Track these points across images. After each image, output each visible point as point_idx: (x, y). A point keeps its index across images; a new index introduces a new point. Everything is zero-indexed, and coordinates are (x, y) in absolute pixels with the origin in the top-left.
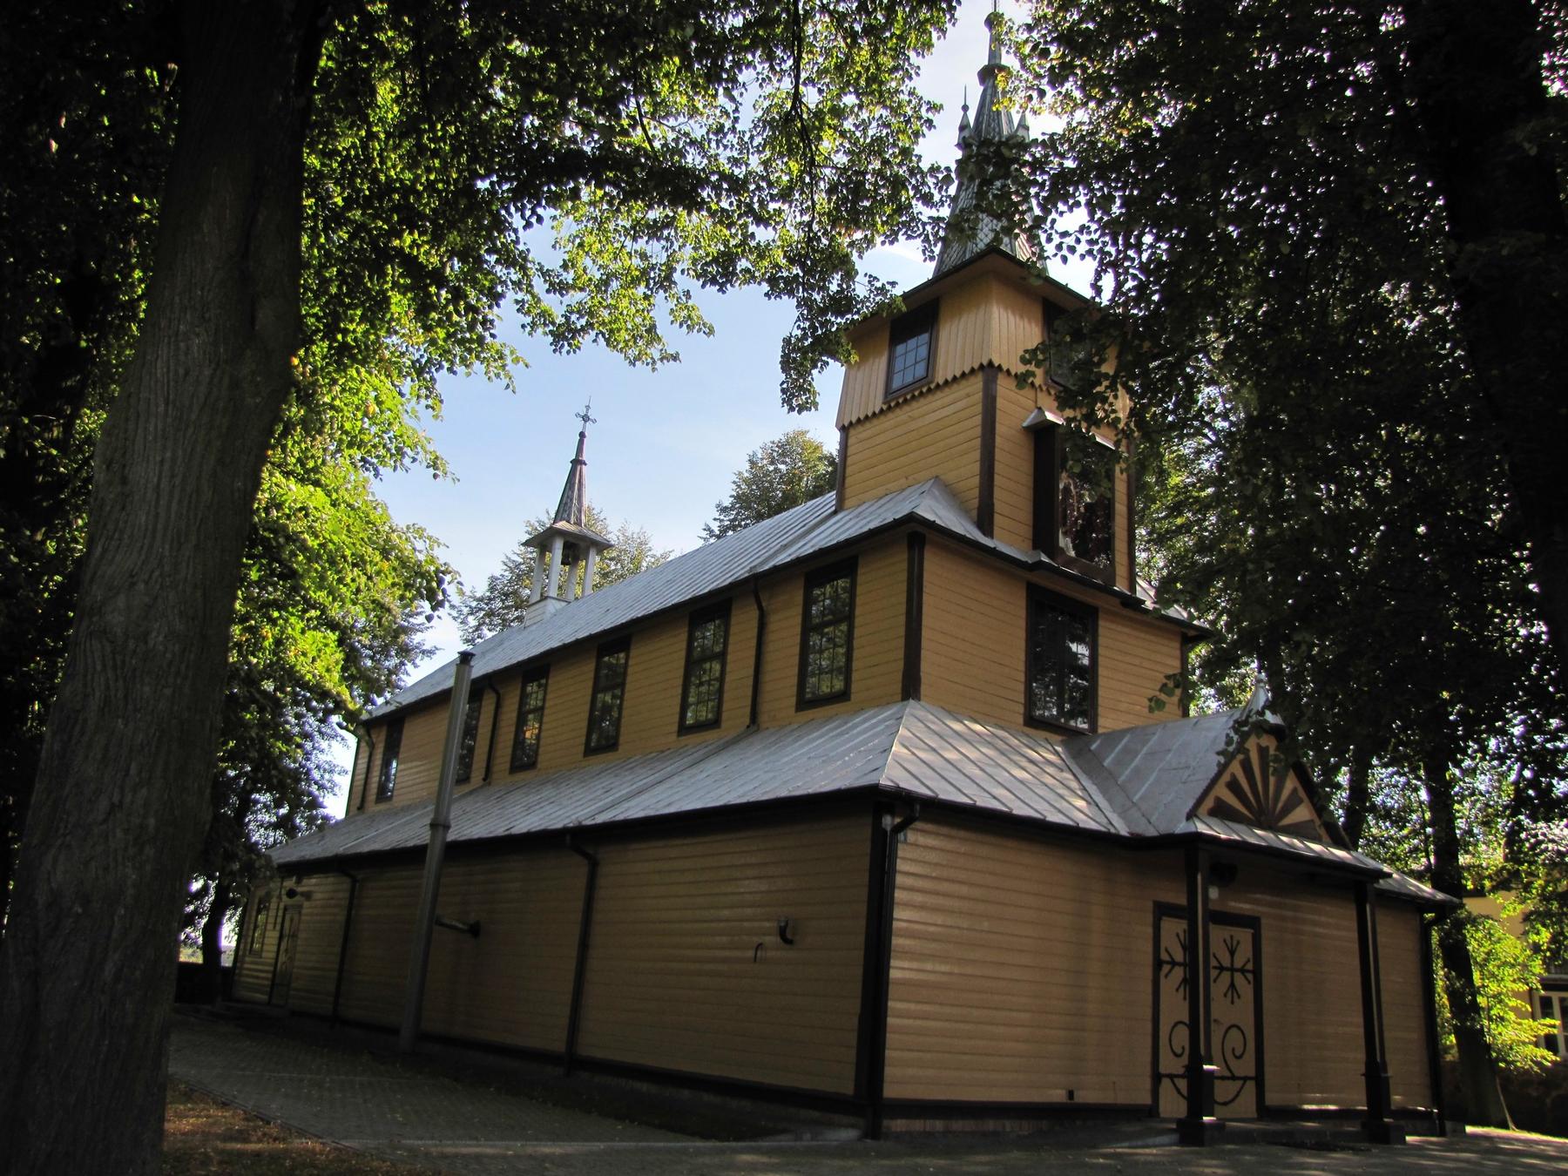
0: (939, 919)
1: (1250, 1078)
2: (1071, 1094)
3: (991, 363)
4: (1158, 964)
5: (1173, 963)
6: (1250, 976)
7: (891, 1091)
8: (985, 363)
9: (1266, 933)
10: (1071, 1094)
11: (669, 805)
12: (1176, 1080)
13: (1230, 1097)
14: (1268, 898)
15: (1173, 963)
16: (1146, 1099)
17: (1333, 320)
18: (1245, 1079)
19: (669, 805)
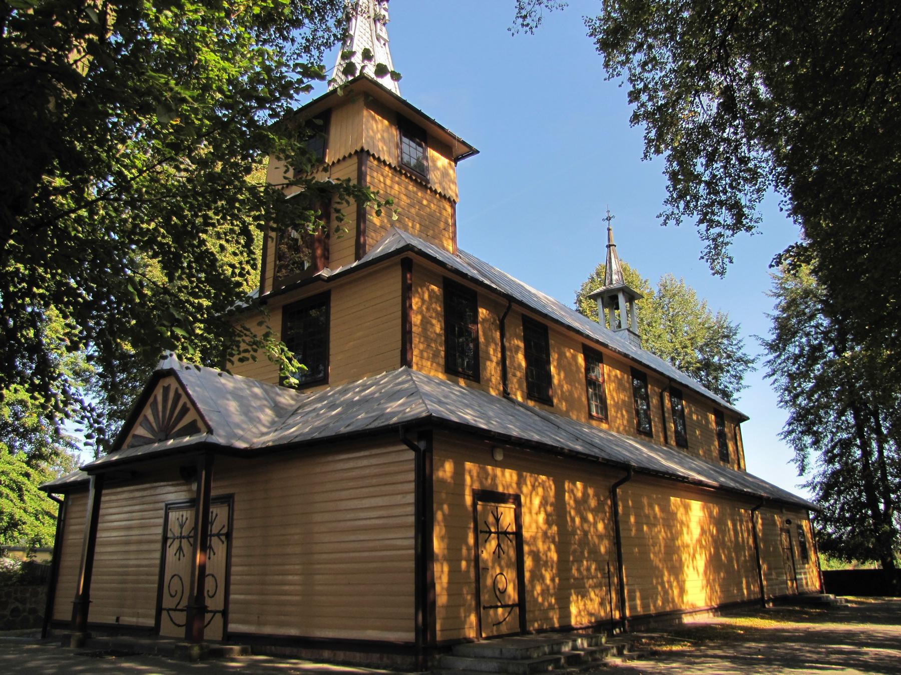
0: (122, 533)
1: (219, 612)
2: (118, 619)
3: (362, 149)
4: (229, 536)
5: (218, 535)
6: (223, 538)
7: (92, 618)
8: (359, 150)
9: (237, 506)
10: (118, 619)
11: (349, 425)
12: (171, 612)
13: (177, 622)
14: (366, 453)
15: (218, 535)
16: (151, 622)
17: (186, 239)
18: (215, 612)
19: (349, 425)
